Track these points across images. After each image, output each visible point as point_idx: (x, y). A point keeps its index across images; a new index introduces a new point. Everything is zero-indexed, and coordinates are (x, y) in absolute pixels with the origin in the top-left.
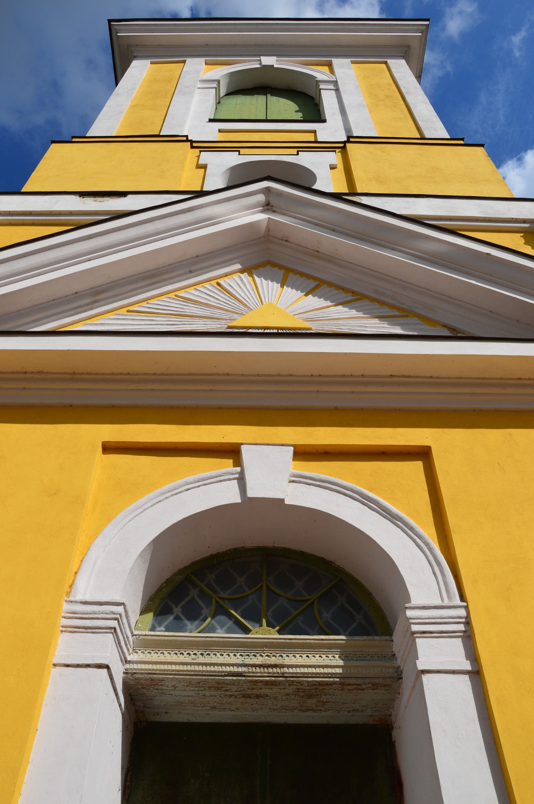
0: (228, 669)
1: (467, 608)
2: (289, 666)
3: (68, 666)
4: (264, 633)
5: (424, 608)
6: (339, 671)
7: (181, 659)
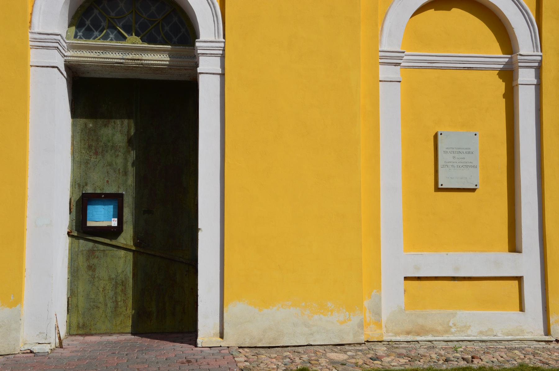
0: (116, 61)
1: (224, 42)
2: (144, 60)
3: (38, 66)
4: (133, 41)
5: (205, 42)
6: (168, 63)
7: (92, 55)
